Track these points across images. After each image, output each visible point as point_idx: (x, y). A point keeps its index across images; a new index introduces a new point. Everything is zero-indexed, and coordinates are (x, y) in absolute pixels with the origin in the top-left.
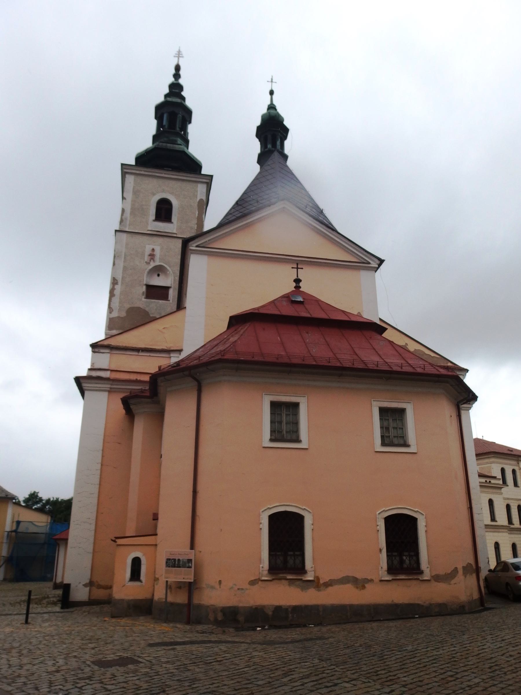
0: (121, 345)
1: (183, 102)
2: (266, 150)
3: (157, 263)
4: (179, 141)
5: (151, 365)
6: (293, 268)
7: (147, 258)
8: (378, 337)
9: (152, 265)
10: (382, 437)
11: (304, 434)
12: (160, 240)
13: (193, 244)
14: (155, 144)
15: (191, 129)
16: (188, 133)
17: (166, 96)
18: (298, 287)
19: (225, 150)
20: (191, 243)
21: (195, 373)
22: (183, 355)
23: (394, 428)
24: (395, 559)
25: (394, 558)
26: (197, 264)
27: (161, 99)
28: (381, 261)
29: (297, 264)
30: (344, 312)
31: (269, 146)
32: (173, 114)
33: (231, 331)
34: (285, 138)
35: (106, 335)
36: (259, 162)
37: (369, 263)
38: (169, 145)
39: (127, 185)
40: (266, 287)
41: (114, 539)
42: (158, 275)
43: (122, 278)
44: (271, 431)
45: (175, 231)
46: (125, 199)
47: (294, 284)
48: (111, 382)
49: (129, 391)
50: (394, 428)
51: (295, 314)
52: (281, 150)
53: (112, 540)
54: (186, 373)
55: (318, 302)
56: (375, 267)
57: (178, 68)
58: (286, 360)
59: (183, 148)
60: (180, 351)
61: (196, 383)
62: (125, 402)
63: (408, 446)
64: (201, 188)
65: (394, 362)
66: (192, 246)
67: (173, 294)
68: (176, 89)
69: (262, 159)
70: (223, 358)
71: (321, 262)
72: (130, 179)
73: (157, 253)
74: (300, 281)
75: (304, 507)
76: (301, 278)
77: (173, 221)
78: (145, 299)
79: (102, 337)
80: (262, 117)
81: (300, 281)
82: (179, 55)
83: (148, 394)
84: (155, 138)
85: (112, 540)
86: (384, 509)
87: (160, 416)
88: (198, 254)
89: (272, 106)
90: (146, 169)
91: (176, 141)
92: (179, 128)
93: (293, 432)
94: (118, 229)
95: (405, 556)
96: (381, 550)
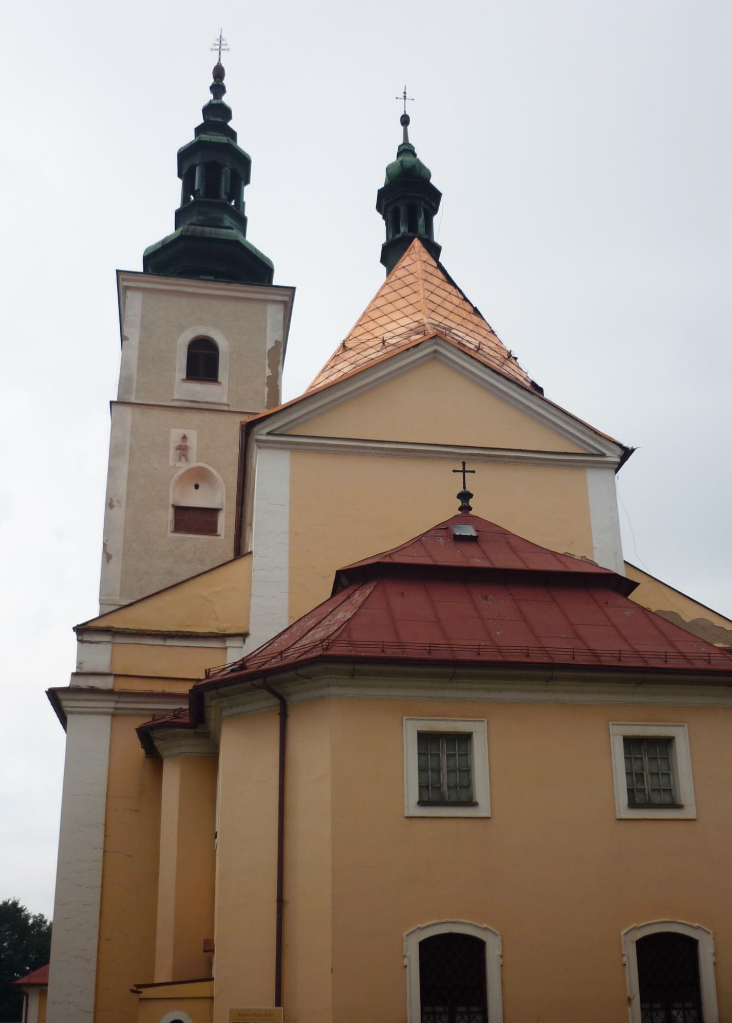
0: (131, 627)
1: (231, 141)
2: (398, 236)
3: (194, 464)
4: (228, 221)
5: (194, 664)
6: (454, 471)
7: (172, 453)
8: (620, 600)
9: (184, 467)
10: (630, 791)
12: (197, 418)
13: (262, 429)
14: (180, 229)
15: (249, 193)
16: (244, 203)
17: (199, 130)
18: (465, 508)
19: (313, 231)
20: (256, 429)
21: (275, 683)
23: (652, 774)
24: (657, 1014)
25: (654, 1014)
26: (272, 471)
27: (189, 137)
28: (627, 453)
29: (464, 463)
30: (554, 554)
31: (403, 229)
32: (214, 166)
33: (340, 597)
34: (435, 210)
35: (102, 603)
36: (384, 260)
37: (604, 455)
38: (207, 229)
39: (129, 313)
40: (401, 511)
41: (135, 988)
42: (197, 487)
43: (128, 496)
44: (420, 787)
45: (225, 400)
46: (127, 339)
47: (459, 503)
48: (116, 698)
50: (652, 774)
52: (426, 237)
53: (132, 991)
54: (258, 682)
55: (504, 535)
56: (614, 463)
57: (219, 73)
58: (445, 655)
59: (234, 233)
60: (244, 636)
61: (276, 701)
62: (146, 735)
63: (680, 807)
64: (274, 313)
65: (651, 649)
66: (260, 434)
67: (226, 523)
68: (217, 115)
69: (391, 255)
71: (509, 457)
72: (135, 300)
73: (193, 442)
74: (471, 496)
75: (485, 926)
77: (220, 379)
78: (172, 523)
79: (96, 614)
80: (387, 169)
81: (471, 496)
82: (220, 46)
83: (186, 720)
85: (132, 991)
86: (635, 925)
87: (210, 760)
88: (271, 448)
91: (221, 220)
92: (226, 193)
93: (461, 787)
94: (115, 399)
95: (676, 1009)
96: (629, 1000)
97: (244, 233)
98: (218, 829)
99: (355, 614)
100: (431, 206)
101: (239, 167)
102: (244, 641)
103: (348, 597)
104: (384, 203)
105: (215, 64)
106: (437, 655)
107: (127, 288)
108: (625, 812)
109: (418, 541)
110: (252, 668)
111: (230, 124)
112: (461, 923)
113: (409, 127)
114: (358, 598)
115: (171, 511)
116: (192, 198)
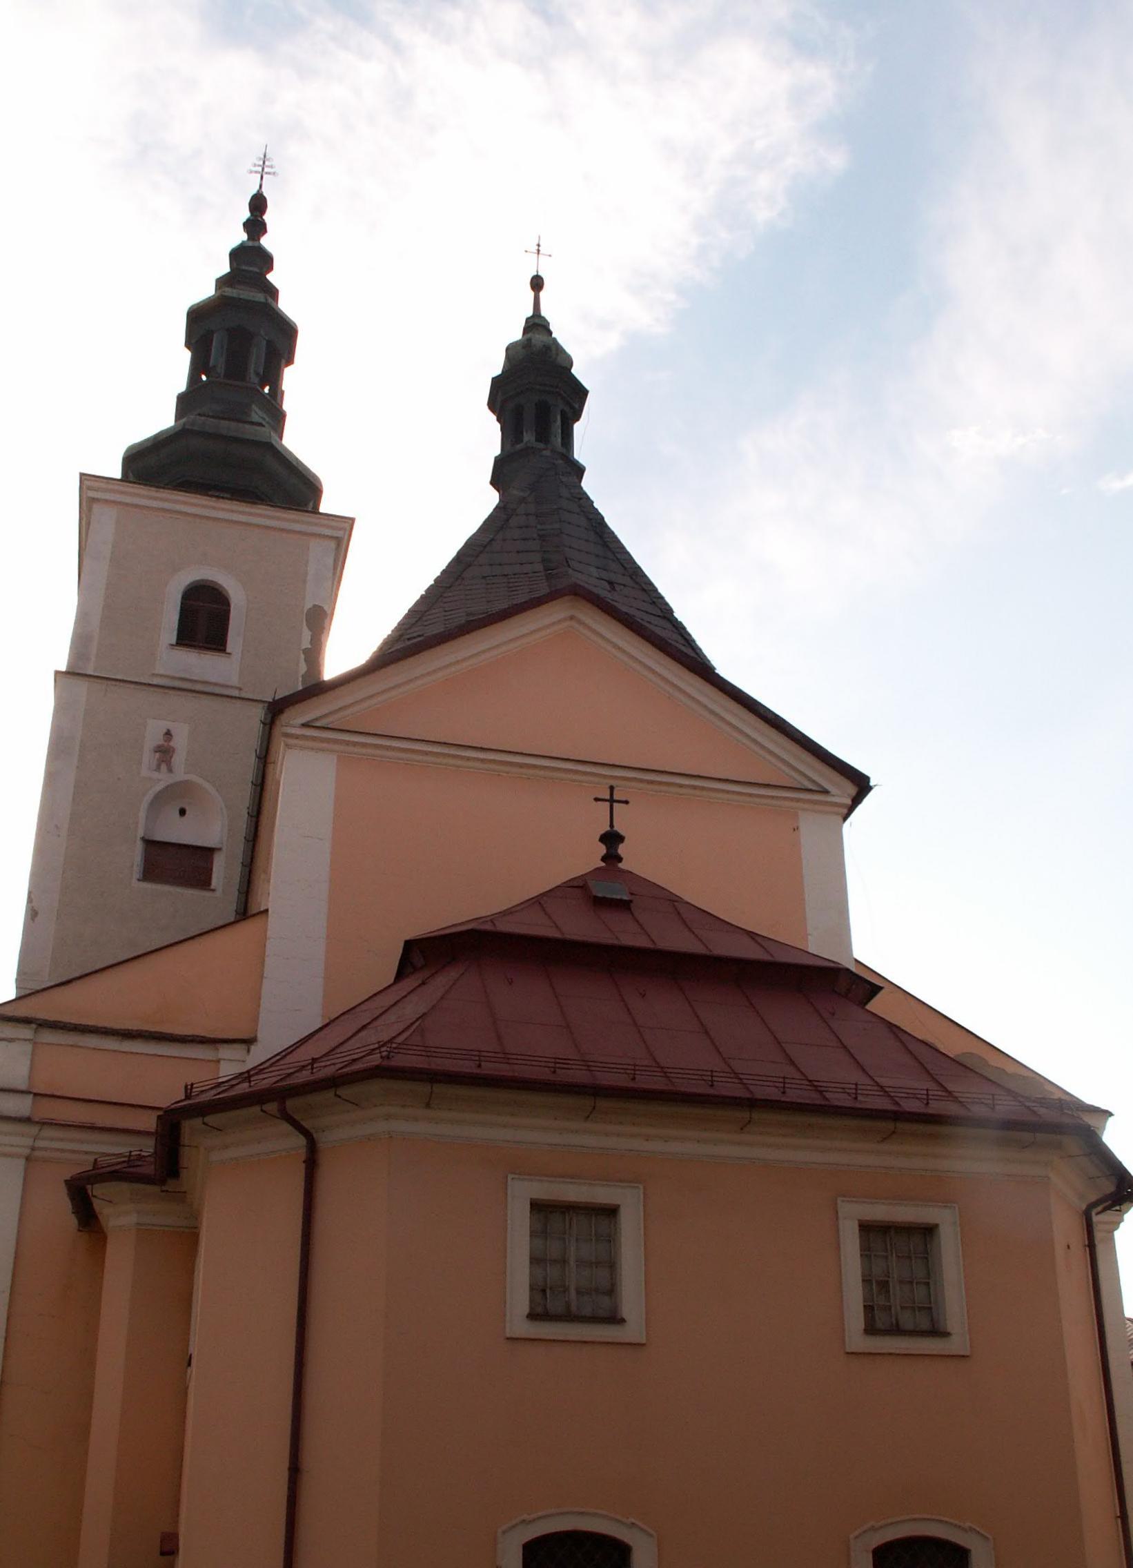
1: (270, 300)
2: (519, 447)
3: (180, 774)
5: (162, 1079)
6: (597, 799)
7: (148, 758)
9: (163, 779)
10: (869, 1309)
11: (631, 1301)
15: (291, 378)
16: (283, 393)
17: (221, 282)
18: (612, 858)
22: (258, 1055)
23: (901, 1282)
26: (308, 786)
27: (206, 290)
30: (752, 935)
32: (240, 334)
33: (409, 983)
34: (577, 416)
37: (826, 792)
38: (224, 423)
42: (182, 812)
45: (235, 681)
48: (34, 1130)
49: (91, 1158)
51: (605, 938)
52: (564, 451)
54: (272, 1107)
57: (258, 204)
58: (578, 1075)
59: (264, 433)
60: (249, 1042)
61: (301, 1141)
62: (80, 1193)
66: (293, 719)
67: (224, 871)
68: (250, 262)
70: (386, 1063)
73: (180, 742)
74: (620, 839)
76: (622, 833)
78: (152, 846)
80: (507, 349)
81: (620, 839)
82: (264, 167)
83: (149, 1170)
84: (185, 403)
86: (872, 1523)
89: (537, 321)
90: (152, 492)
92: (257, 374)
97: (281, 438)
98: (194, 1349)
99: (434, 1007)
100: (572, 407)
101: (280, 339)
102: (249, 1051)
103: (423, 983)
104: (499, 399)
105: (254, 191)
106: (563, 1076)
107: (94, 500)
108: (856, 1338)
109: (538, 901)
110: (264, 1082)
111: (270, 277)
112: (595, 1515)
113: (542, 294)
114: (441, 981)
115: (139, 846)
116: (204, 378)
